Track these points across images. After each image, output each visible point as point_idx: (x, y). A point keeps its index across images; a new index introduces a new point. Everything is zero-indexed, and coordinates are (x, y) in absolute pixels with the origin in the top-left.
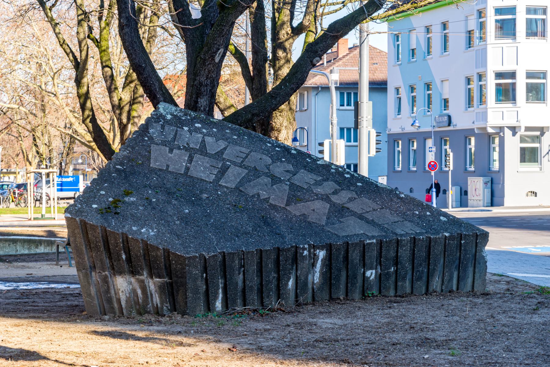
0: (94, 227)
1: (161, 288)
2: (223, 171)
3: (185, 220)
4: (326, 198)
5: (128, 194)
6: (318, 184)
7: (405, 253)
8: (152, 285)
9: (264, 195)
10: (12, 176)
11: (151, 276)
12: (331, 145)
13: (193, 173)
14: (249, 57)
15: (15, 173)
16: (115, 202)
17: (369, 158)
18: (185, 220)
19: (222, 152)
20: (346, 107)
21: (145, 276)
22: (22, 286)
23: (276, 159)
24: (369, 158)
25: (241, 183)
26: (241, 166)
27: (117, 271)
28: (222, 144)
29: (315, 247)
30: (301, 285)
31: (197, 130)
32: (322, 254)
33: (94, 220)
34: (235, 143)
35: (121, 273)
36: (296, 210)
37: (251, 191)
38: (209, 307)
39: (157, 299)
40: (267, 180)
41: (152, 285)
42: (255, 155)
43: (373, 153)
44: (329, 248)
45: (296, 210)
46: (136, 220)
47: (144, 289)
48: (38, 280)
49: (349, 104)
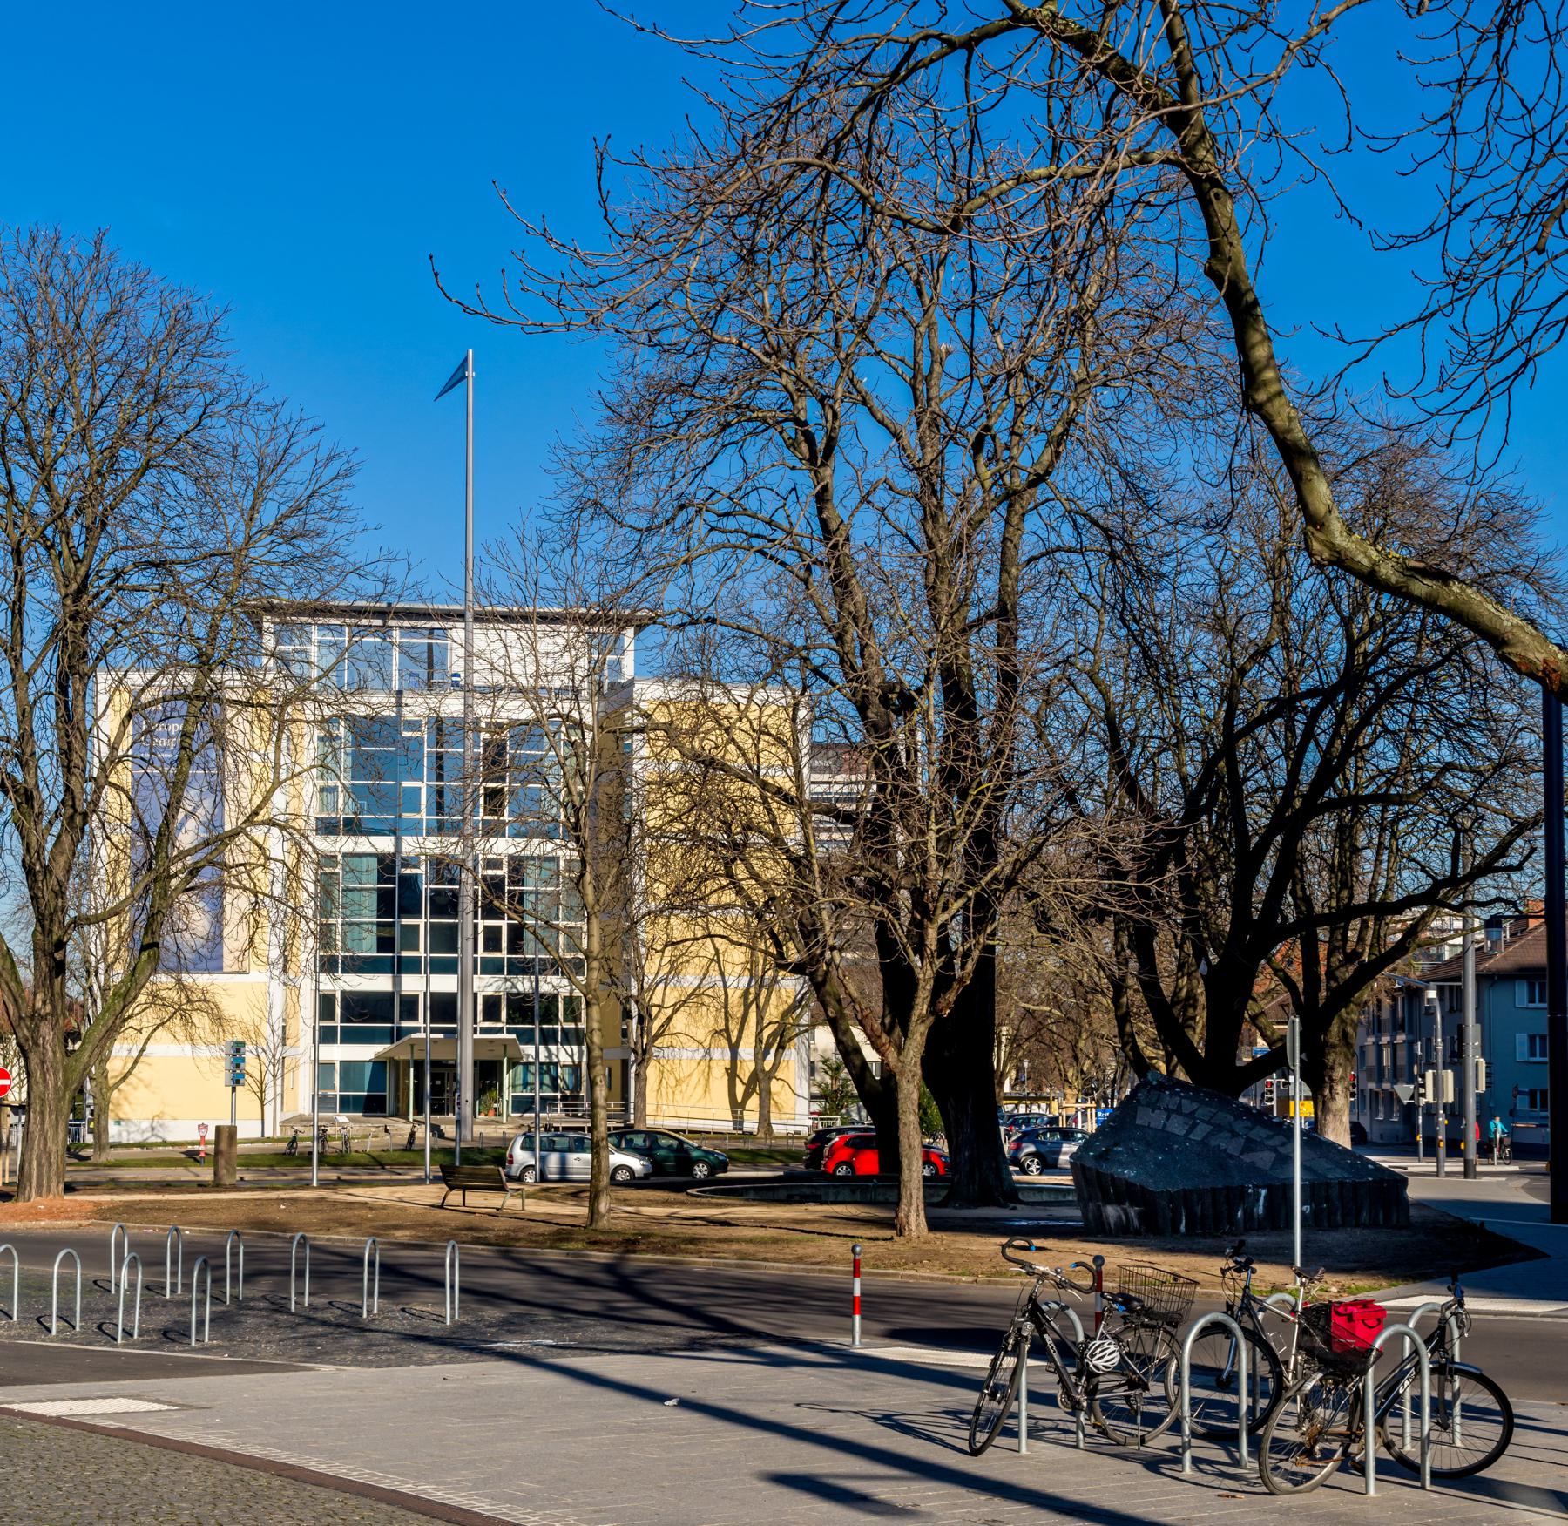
0: (1090, 1169)
1: (1140, 1215)
2: (1192, 1128)
3: (1159, 1165)
4: (1274, 1149)
5: (1116, 1144)
6: (1269, 1137)
7: (1335, 1192)
8: (1132, 1212)
9: (1223, 1146)
10: (1043, 1105)
11: (1132, 1205)
12: (1435, 1078)
13: (1169, 1129)
14: (1301, 986)
15: (1047, 1099)
16: (1107, 1151)
17: (1478, 1095)
18: (1159, 1165)
19: (1193, 1112)
20: (1537, 1005)
21: (1127, 1206)
22: (1043, 1223)
23: (1238, 1117)
24: (1478, 1095)
25: (1207, 1136)
26: (1208, 1123)
27: (1108, 1202)
28: (1195, 1106)
29: (1259, 1187)
30: (1249, 1215)
31: (1177, 1094)
32: (1263, 1192)
33: (1090, 1164)
34: (1207, 1104)
35: (1110, 1203)
36: (1247, 1158)
37: (1213, 1143)
38: (1176, 1230)
39: (1136, 1222)
40: (1228, 1135)
41: (1132, 1212)
42: (1222, 1115)
43: (1483, 1088)
44: (1269, 1188)
45: (1247, 1158)
46: (1122, 1164)
47: (1127, 1214)
48: (1058, 1219)
49: (1541, 1001)
